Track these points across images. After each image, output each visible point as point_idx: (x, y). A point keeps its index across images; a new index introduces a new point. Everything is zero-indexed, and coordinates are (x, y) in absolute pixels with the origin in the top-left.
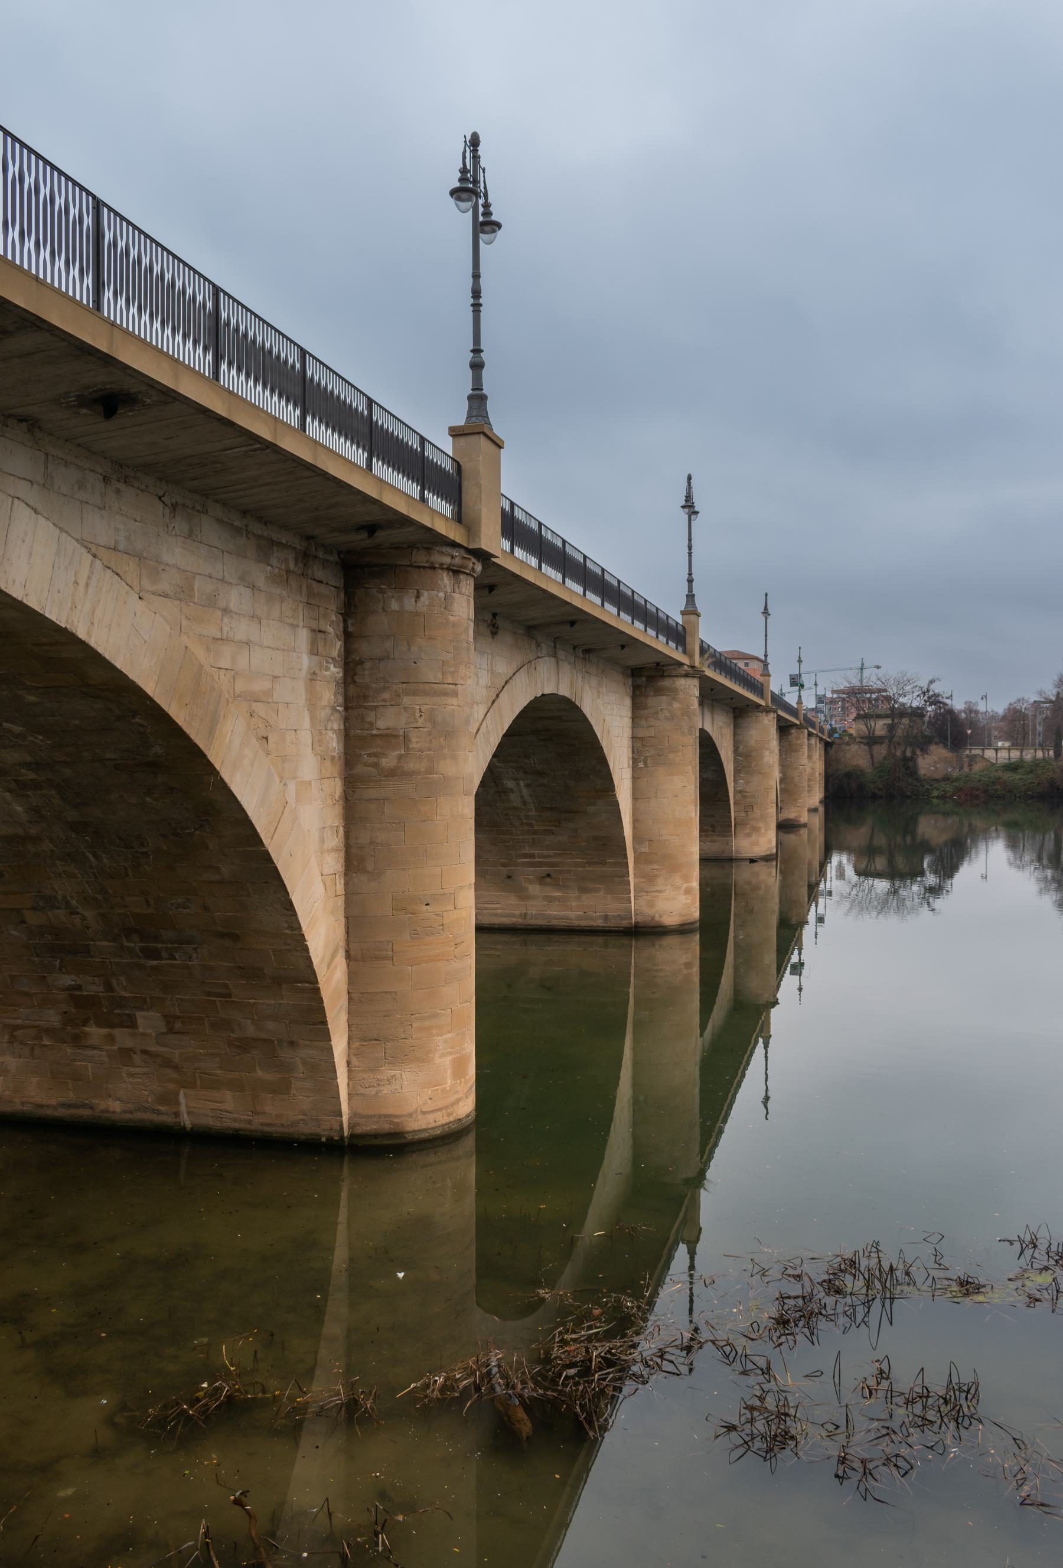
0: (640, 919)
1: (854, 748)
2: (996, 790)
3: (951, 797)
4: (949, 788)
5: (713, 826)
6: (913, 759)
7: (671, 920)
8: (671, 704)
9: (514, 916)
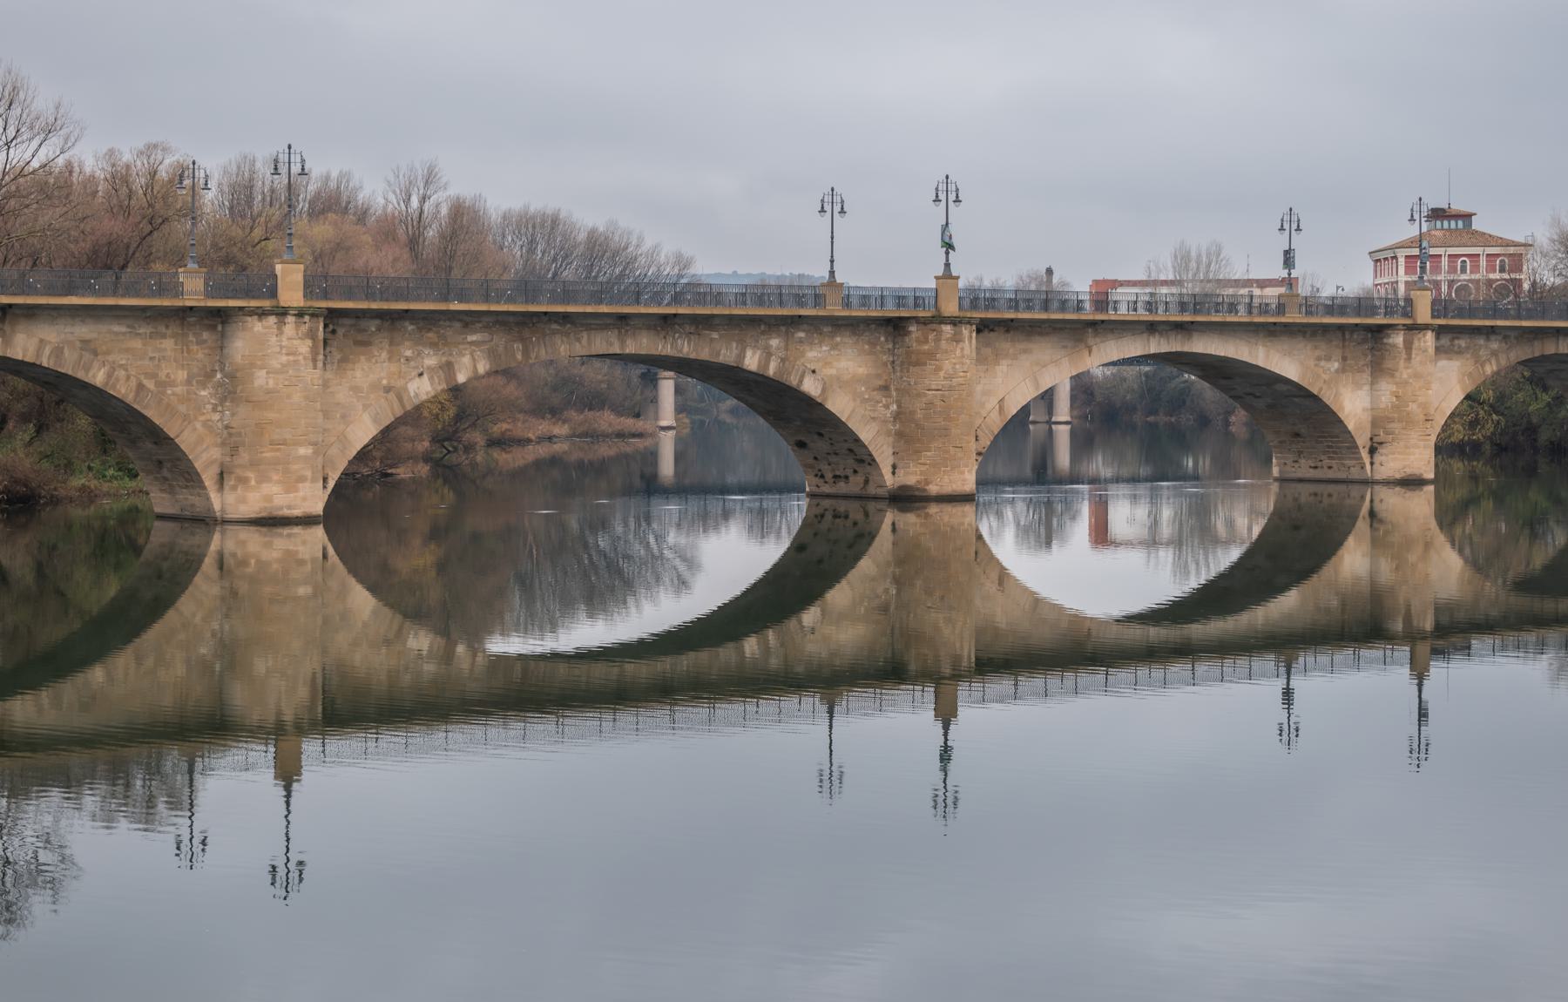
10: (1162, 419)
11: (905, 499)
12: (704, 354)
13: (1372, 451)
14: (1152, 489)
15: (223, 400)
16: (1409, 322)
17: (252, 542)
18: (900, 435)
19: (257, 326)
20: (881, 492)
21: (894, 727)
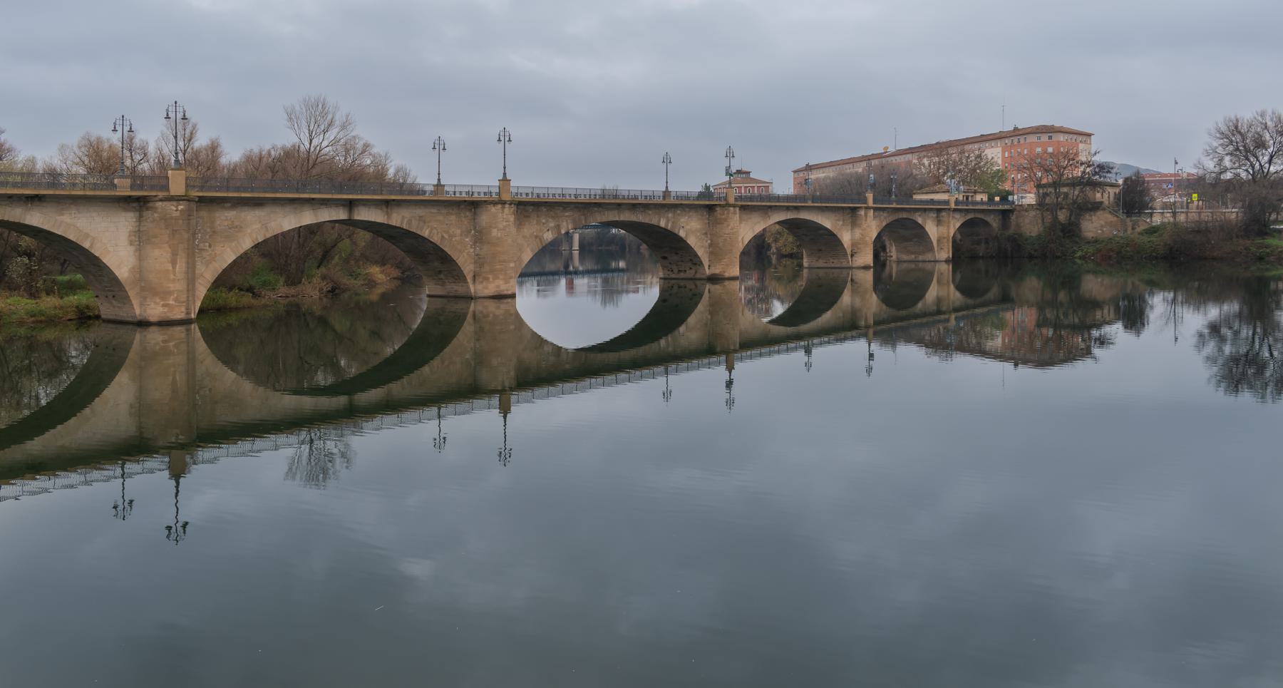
6: (1078, 225)
7: (153, 319)
10: (603, 248)
11: (714, 279)
12: (622, 218)
14: (606, 282)
15: (475, 242)
17: (491, 306)
18: (711, 253)
19: (493, 209)
21: (710, 376)
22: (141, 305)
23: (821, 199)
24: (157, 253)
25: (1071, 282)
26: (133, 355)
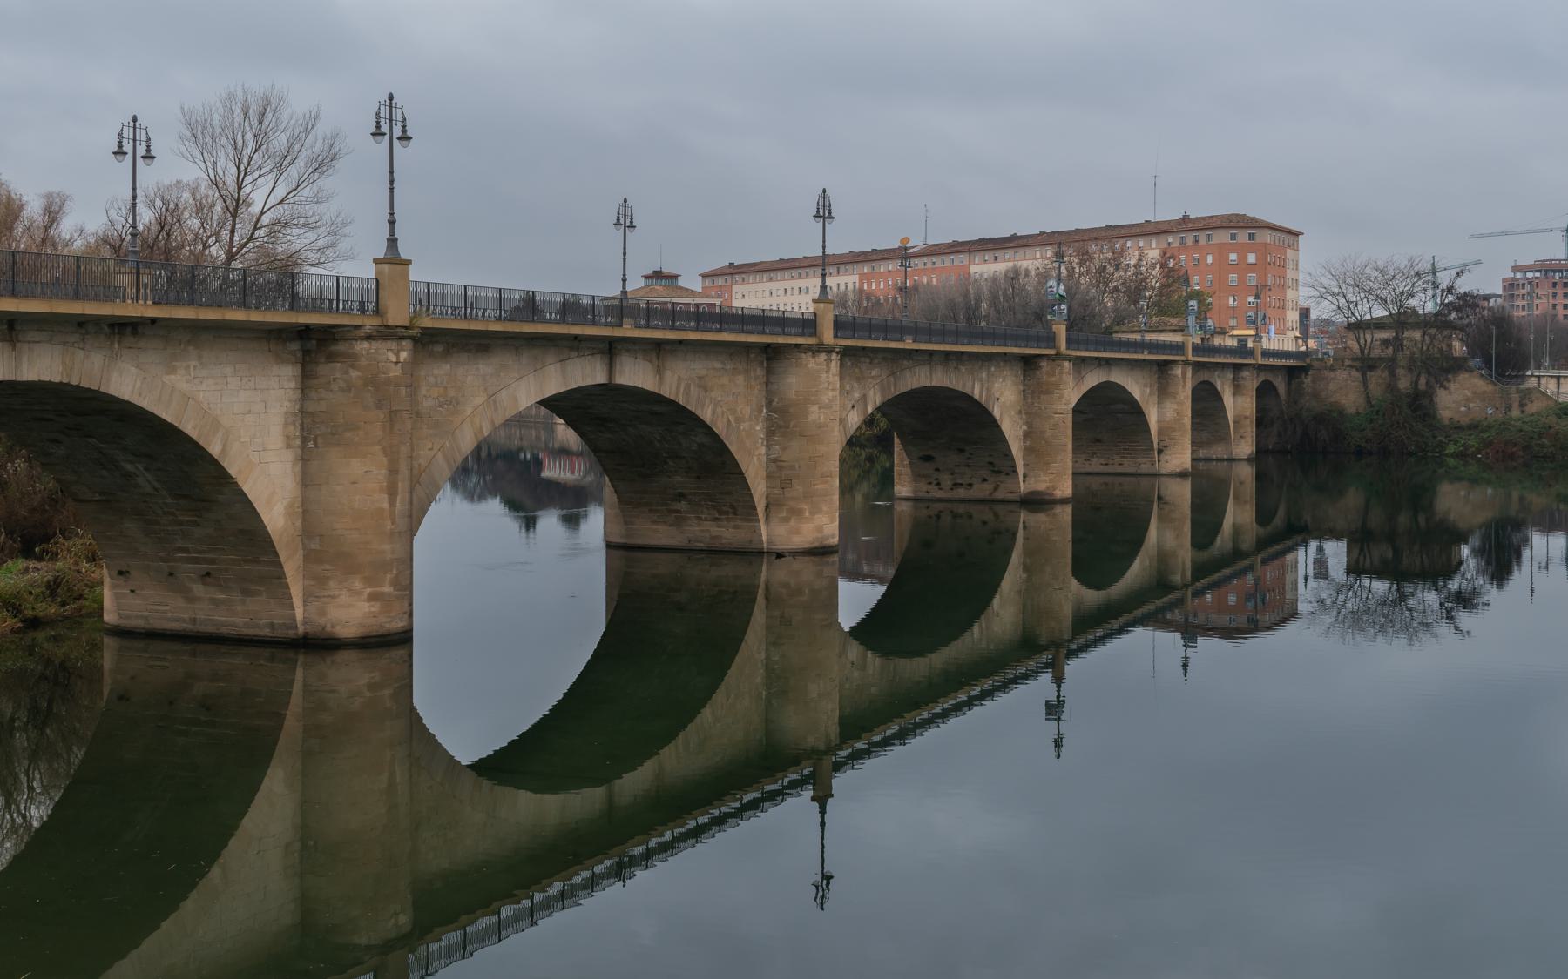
0: (310, 629)
1: (1341, 375)
2: (1543, 446)
3: (1473, 456)
4: (1473, 442)
5: (732, 506)
6: (1429, 394)
7: (347, 632)
8: (347, 372)
9: (184, 621)
13: (1160, 452)
16: (1053, 352)
20: (1010, 496)
22: (307, 597)
23: (928, 333)
24: (356, 467)
25: (1421, 498)
26: (292, 724)
